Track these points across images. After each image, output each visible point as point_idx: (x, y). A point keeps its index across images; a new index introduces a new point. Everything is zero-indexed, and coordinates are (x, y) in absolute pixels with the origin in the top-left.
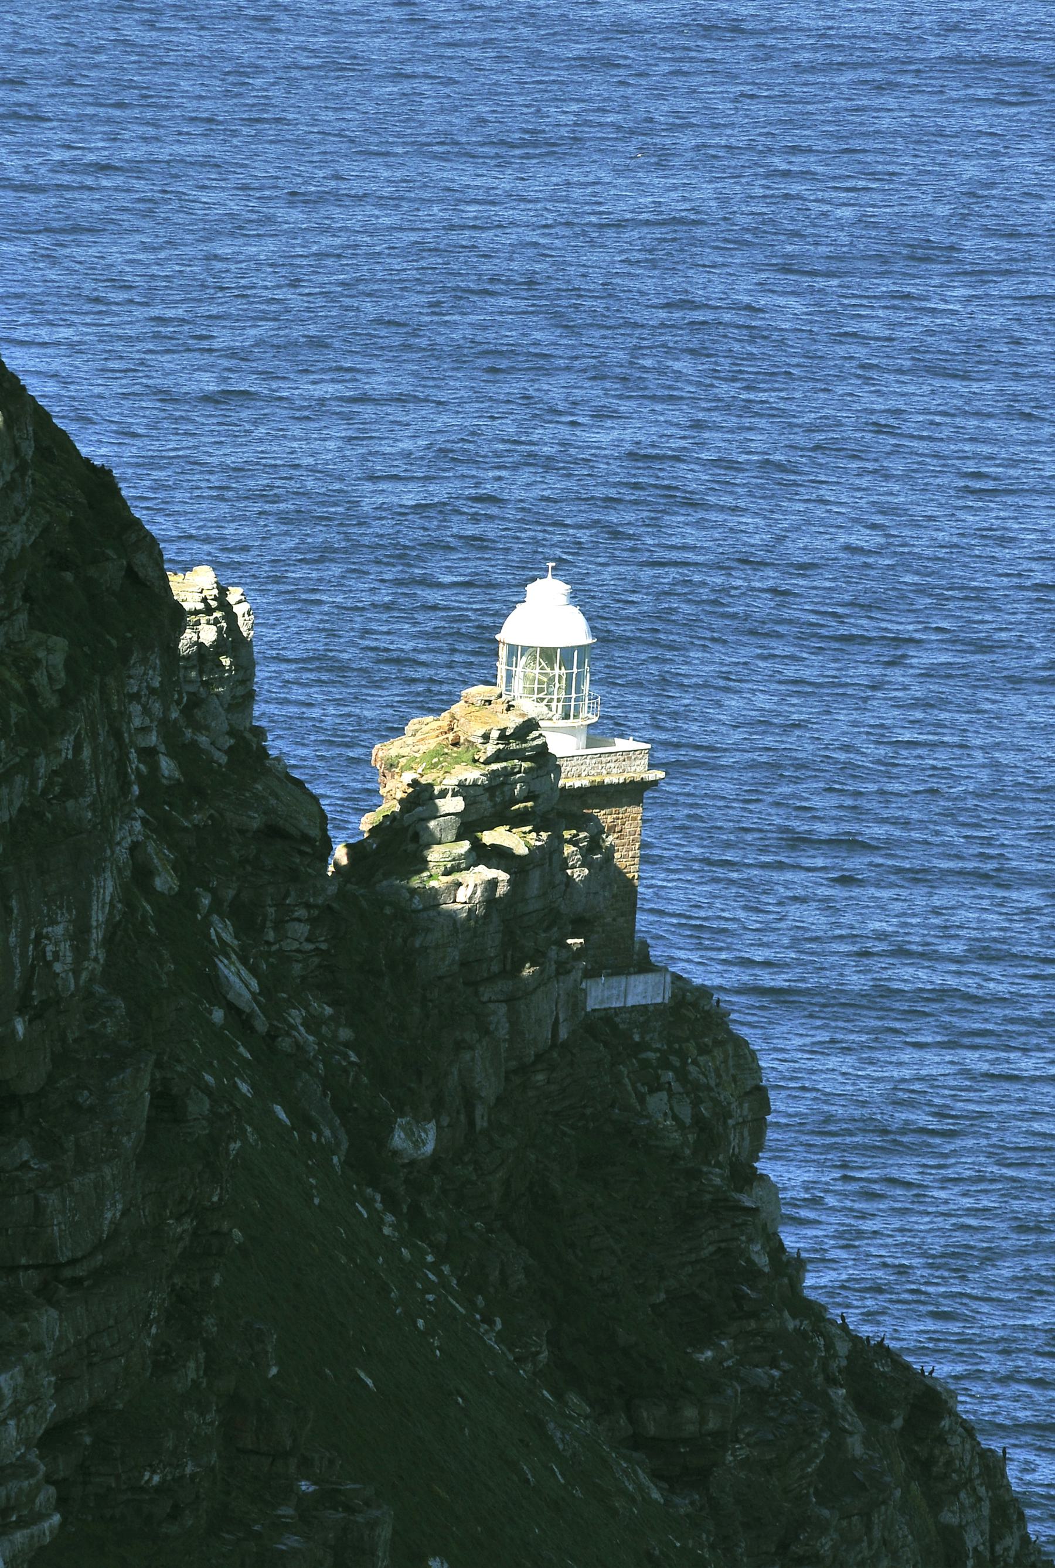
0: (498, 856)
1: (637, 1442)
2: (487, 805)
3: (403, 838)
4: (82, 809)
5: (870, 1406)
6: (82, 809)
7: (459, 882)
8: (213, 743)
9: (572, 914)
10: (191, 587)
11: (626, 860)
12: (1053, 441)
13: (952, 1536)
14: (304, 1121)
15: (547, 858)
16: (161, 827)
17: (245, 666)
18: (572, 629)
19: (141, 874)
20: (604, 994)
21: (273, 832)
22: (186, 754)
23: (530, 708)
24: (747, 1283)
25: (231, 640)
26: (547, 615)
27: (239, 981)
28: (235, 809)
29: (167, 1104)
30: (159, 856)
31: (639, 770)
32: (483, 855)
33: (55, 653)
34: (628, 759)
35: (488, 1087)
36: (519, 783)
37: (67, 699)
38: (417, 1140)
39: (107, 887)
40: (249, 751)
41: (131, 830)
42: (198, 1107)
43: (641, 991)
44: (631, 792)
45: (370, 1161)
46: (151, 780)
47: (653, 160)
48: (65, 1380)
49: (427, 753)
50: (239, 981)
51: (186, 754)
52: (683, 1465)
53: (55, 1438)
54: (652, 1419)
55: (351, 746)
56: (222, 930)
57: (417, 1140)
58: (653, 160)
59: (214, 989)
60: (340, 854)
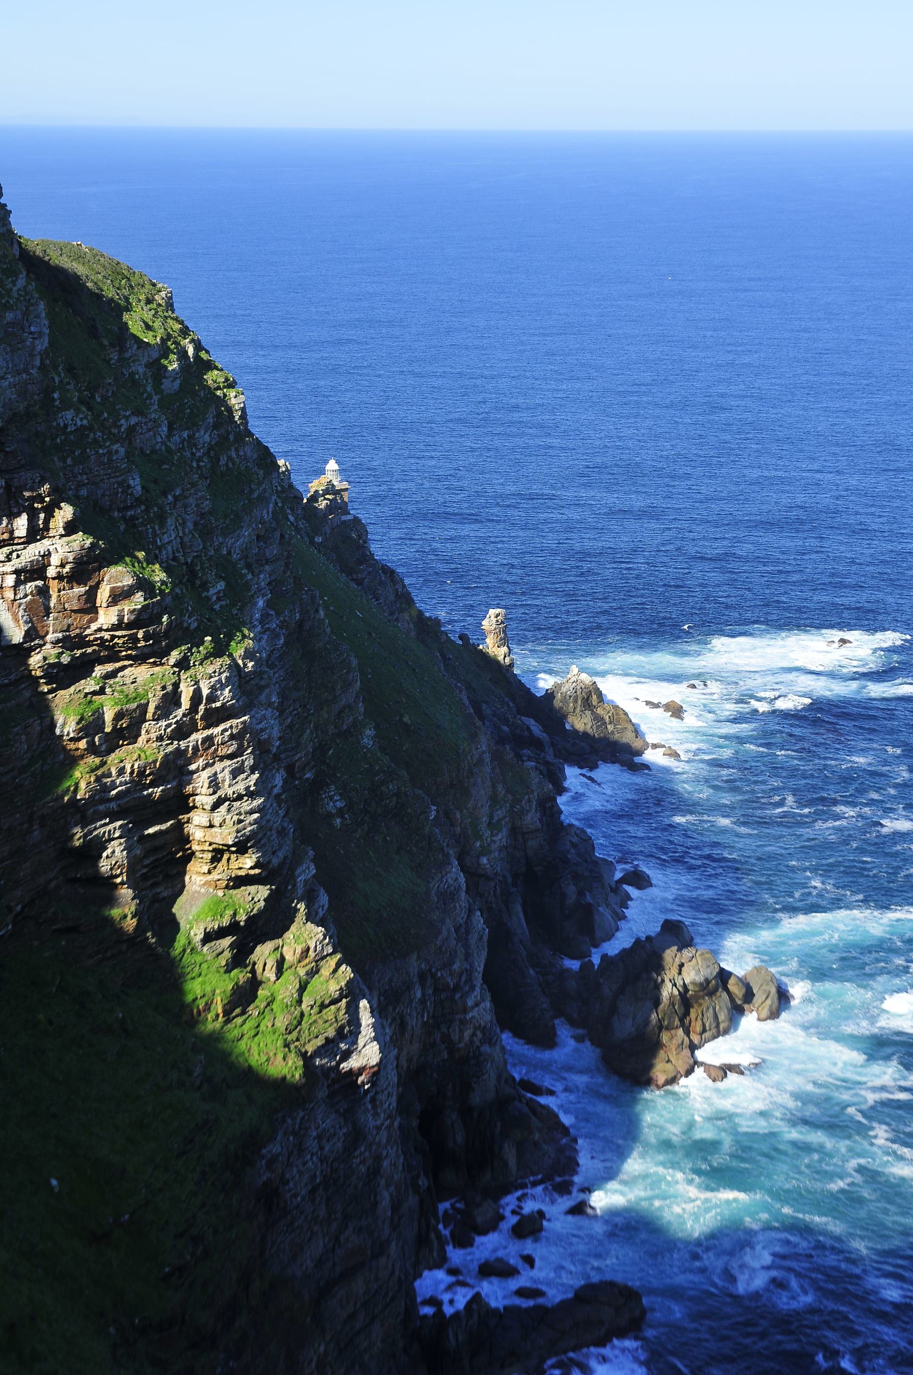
0: (328, 499)
1: (353, 580)
2: (326, 492)
3: (314, 498)
4: (267, 495)
5: (385, 572)
6: (267, 495)
7: (322, 504)
8: (286, 485)
9: (338, 507)
10: (281, 462)
11: (346, 499)
12: (910, 649)
13: (397, 590)
14: (302, 538)
15: (335, 499)
16: (279, 497)
17: (289, 474)
18: (336, 467)
19: (276, 503)
20: (344, 518)
21: (295, 497)
22: (282, 486)
23: (331, 478)
24: (366, 557)
25: (287, 470)
26: (332, 465)
27: (291, 518)
28: (290, 495)
29: (282, 536)
30: (279, 501)
31: (347, 487)
32: (325, 499)
33: (261, 472)
34: (345, 485)
35: (328, 531)
36: (330, 489)
37: (264, 479)
38: (318, 539)
39: (271, 505)
40: (291, 486)
41: (274, 497)
42: (287, 536)
43: (349, 517)
44: (346, 490)
45: (312, 543)
46: (277, 490)
47: (861, 897)
48: (270, 576)
49: (317, 485)
50: (291, 518)
51: (282, 486)
52: (359, 582)
53: (269, 584)
54: (355, 576)
55: (306, 483)
56: (288, 511)
57: (318, 539)
58: (861, 897)
59: (288, 519)
60: (305, 501)
